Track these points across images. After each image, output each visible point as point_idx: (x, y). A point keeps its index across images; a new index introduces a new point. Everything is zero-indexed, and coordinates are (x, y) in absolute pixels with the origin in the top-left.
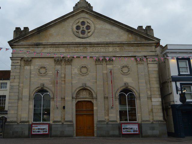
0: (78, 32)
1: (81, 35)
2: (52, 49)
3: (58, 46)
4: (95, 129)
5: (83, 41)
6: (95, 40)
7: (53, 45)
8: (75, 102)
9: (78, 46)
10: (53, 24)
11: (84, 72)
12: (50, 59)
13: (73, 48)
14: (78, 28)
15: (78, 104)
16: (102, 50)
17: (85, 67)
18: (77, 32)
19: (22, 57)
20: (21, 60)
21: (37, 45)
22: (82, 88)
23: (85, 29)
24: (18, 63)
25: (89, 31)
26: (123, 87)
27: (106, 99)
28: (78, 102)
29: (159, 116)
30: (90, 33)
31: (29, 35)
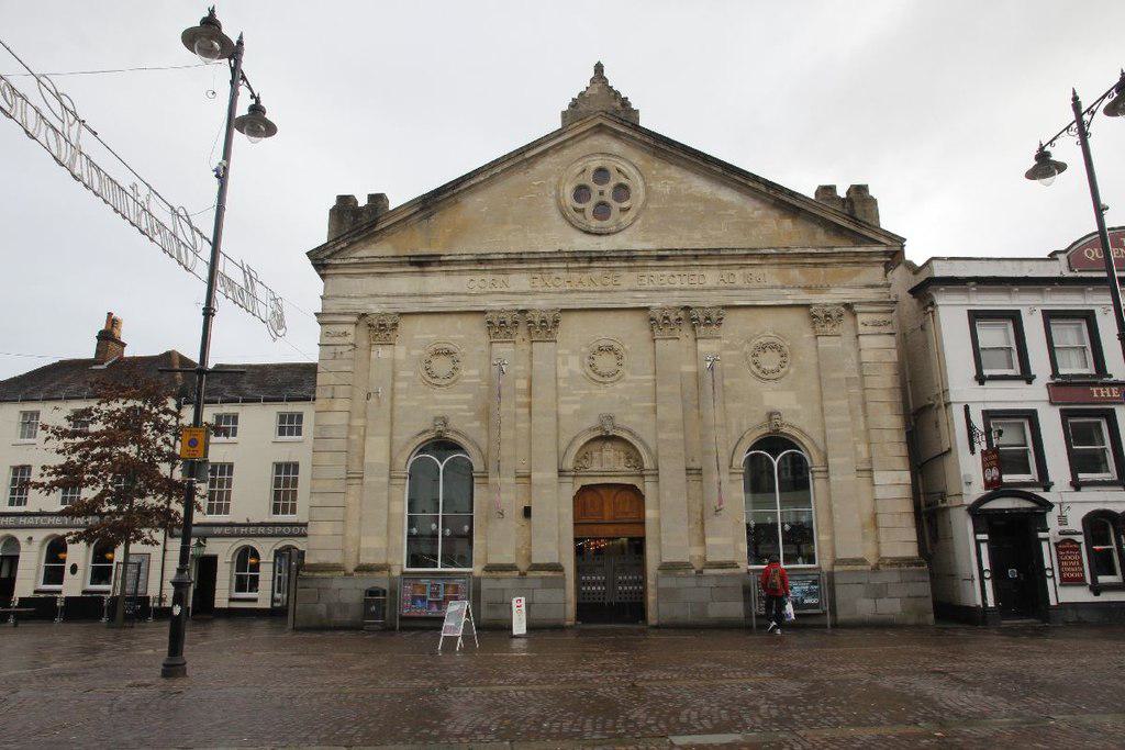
1: (595, 224)
5: (604, 244)
8: (570, 489)
13: (563, 274)
14: (581, 192)
15: (586, 497)
21: (480, 262)
22: (598, 433)
24: (345, 334)
25: (625, 205)
28: (584, 488)
30: (631, 214)
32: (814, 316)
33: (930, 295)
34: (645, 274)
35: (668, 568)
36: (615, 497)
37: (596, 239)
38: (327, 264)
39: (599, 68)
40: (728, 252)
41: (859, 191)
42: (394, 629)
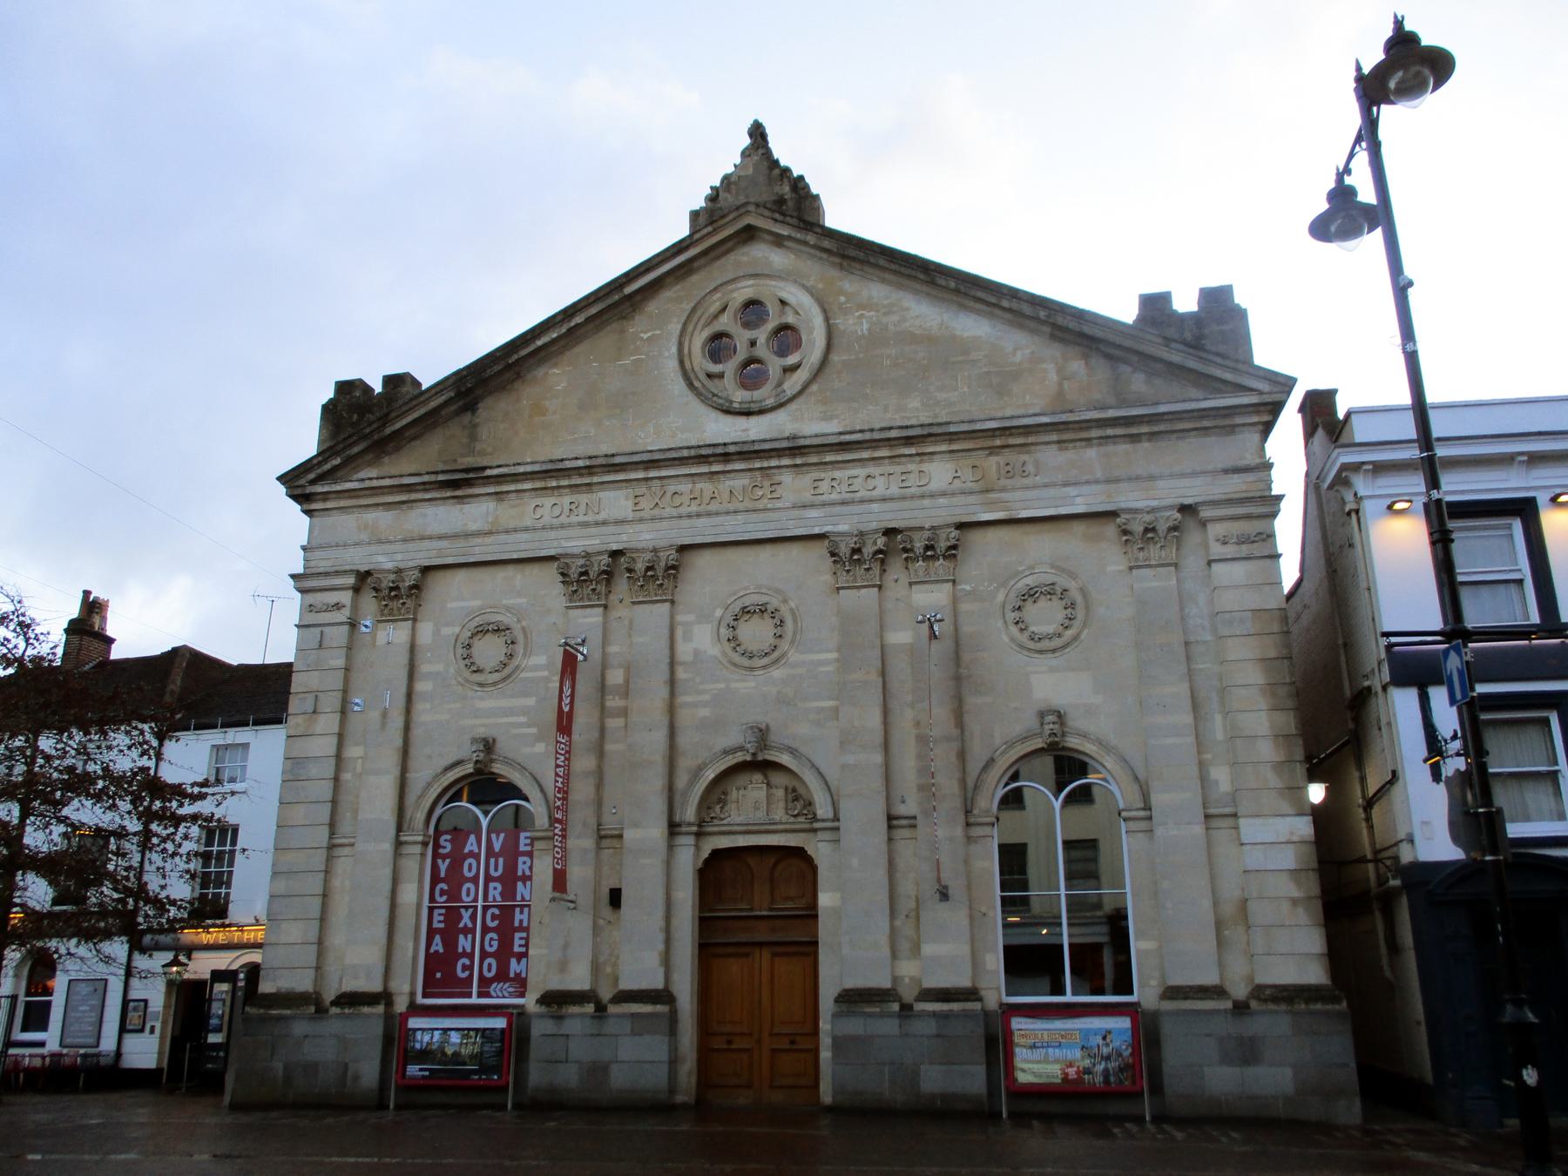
0: (721, 376)
1: (739, 396)
2: (548, 502)
3: (587, 480)
4: (825, 1055)
5: (755, 429)
6: (827, 418)
7: (553, 474)
8: (688, 859)
9: (715, 468)
10: (555, 335)
11: (753, 647)
12: (534, 571)
13: (685, 487)
14: (718, 345)
15: (719, 873)
16: (881, 487)
17: (763, 610)
18: (710, 376)
19: (363, 568)
20: (356, 590)
22: (740, 757)
23: (762, 351)
24: (338, 606)
25: (792, 360)
26: (1024, 739)
27: (905, 833)
28: (717, 854)
29: (1295, 953)
30: (801, 376)
31: (404, 422)
32: (1125, 532)
34: (823, 475)
35: (852, 999)
36: (775, 865)
37: (742, 422)
39: (758, 133)
40: (965, 427)
41: (1218, 302)
42: (995, 1116)
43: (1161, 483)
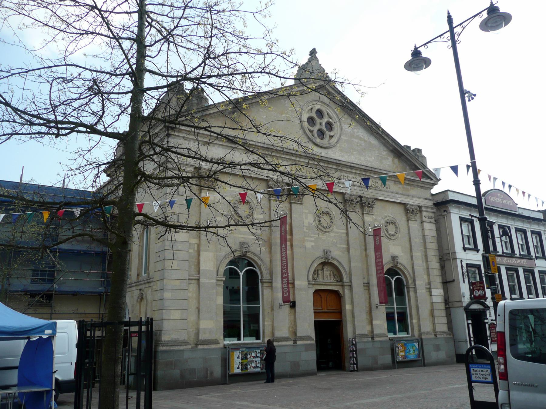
3: (277, 155)
6: (343, 156)
8: (311, 291)
14: (311, 120)
25: (332, 133)
30: (334, 140)
33: (447, 207)
38: (175, 128)
39: (313, 53)
43: (414, 199)
